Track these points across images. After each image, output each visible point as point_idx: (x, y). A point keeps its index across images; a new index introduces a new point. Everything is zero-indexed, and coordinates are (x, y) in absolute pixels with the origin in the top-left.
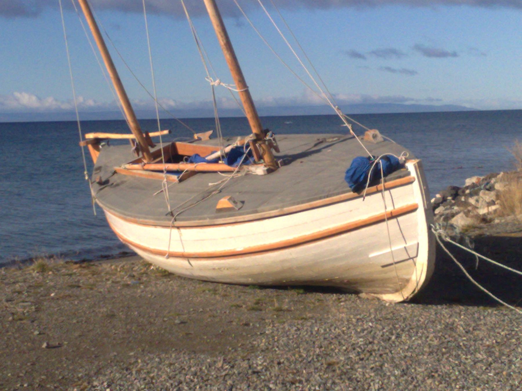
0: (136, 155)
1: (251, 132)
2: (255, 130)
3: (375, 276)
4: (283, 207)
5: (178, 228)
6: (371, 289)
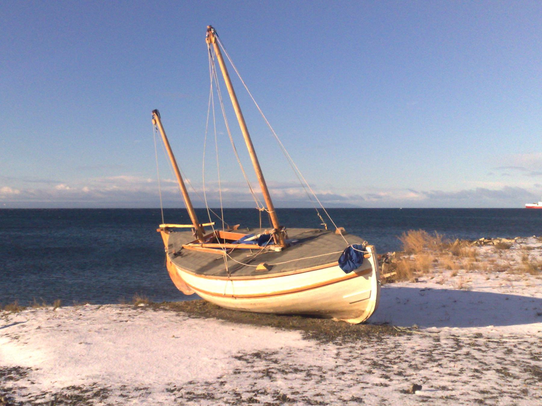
0: (195, 238)
1: (273, 227)
2: (275, 227)
3: (345, 309)
4: (296, 270)
5: (232, 280)
6: (341, 316)
